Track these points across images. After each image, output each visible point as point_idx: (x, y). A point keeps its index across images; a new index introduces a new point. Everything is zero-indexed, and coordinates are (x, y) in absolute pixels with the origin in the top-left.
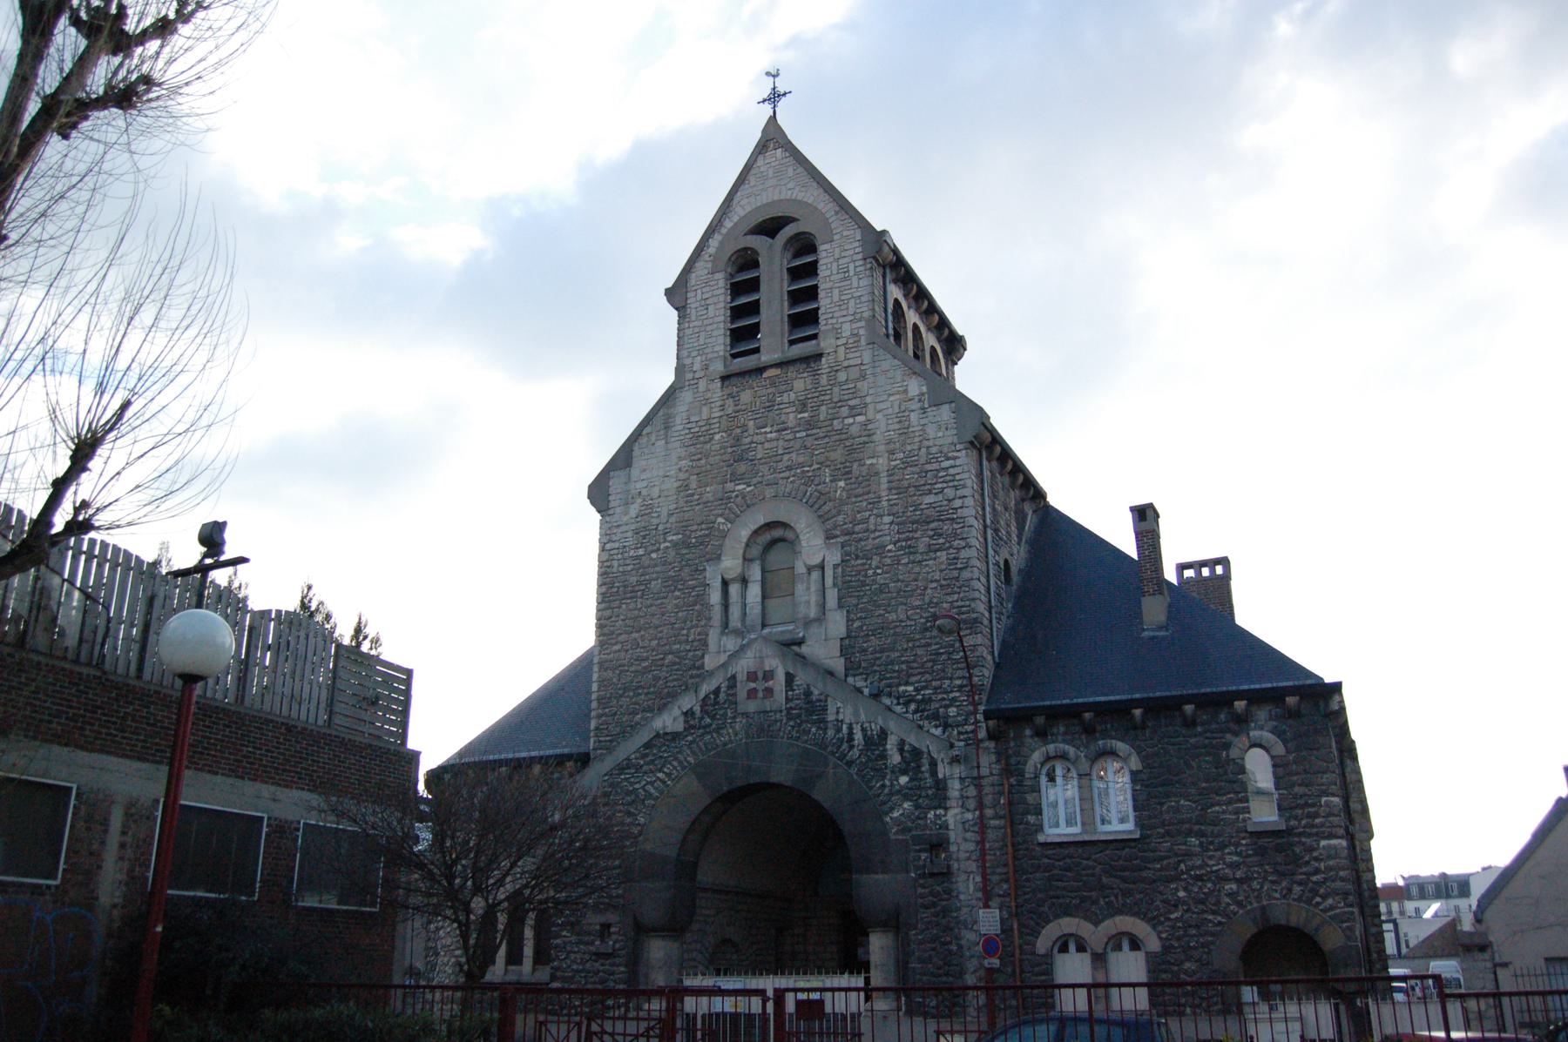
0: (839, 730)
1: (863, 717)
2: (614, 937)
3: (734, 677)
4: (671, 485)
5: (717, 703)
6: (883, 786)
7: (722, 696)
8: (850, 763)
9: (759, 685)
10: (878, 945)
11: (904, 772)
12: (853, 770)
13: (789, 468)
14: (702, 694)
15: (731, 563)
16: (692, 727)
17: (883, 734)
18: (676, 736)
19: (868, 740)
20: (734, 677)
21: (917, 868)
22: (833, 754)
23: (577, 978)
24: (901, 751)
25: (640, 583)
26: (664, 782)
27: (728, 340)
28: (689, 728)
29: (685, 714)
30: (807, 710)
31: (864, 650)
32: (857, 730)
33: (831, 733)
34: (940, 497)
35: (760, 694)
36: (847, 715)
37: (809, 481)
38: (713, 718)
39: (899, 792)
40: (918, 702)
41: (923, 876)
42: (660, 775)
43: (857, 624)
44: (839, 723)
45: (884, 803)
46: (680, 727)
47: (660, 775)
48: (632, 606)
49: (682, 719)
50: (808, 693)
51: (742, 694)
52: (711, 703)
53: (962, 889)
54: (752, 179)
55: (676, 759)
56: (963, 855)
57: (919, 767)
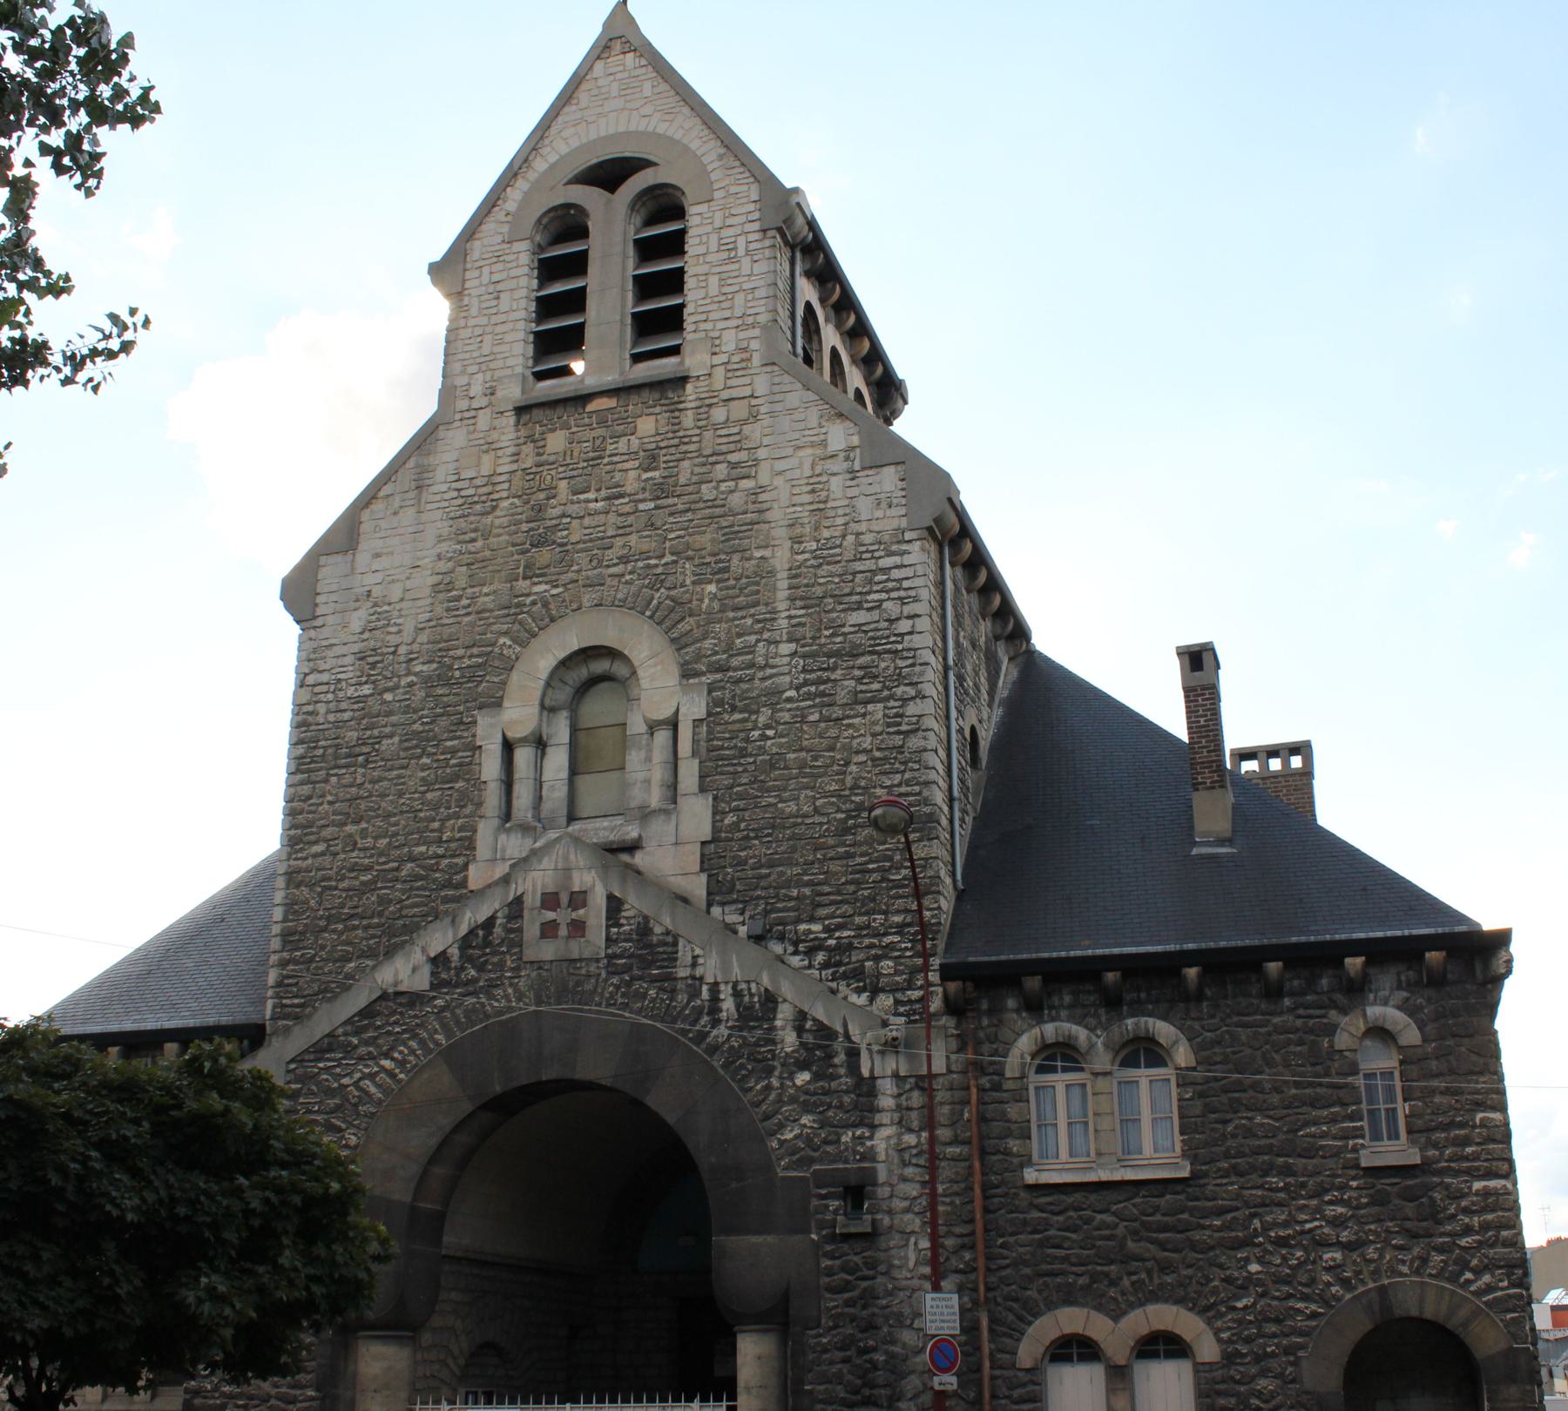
0: (695, 993)
1: (736, 972)
3: (519, 900)
5: (487, 943)
6: (768, 1088)
8: (714, 1049)
9: (562, 916)
11: (803, 1066)
15: (520, 712)
16: (447, 983)
17: (770, 1001)
18: (414, 999)
19: (746, 1015)
20: (519, 900)
21: (820, 1228)
27: (531, 348)
29: (434, 961)
32: (726, 992)
33: (682, 998)
36: (710, 969)
37: (658, 582)
38: (481, 968)
39: (793, 1100)
42: (387, 1063)
43: (730, 819)
45: (767, 1117)
46: (422, 982)
47: (387, 1063)
48: (347, 779)
49: (426, 970)
50: (644, 930)
51: (531, 930)
54: (583, 96)
55: (415, 1036)
57: (830, 1056)
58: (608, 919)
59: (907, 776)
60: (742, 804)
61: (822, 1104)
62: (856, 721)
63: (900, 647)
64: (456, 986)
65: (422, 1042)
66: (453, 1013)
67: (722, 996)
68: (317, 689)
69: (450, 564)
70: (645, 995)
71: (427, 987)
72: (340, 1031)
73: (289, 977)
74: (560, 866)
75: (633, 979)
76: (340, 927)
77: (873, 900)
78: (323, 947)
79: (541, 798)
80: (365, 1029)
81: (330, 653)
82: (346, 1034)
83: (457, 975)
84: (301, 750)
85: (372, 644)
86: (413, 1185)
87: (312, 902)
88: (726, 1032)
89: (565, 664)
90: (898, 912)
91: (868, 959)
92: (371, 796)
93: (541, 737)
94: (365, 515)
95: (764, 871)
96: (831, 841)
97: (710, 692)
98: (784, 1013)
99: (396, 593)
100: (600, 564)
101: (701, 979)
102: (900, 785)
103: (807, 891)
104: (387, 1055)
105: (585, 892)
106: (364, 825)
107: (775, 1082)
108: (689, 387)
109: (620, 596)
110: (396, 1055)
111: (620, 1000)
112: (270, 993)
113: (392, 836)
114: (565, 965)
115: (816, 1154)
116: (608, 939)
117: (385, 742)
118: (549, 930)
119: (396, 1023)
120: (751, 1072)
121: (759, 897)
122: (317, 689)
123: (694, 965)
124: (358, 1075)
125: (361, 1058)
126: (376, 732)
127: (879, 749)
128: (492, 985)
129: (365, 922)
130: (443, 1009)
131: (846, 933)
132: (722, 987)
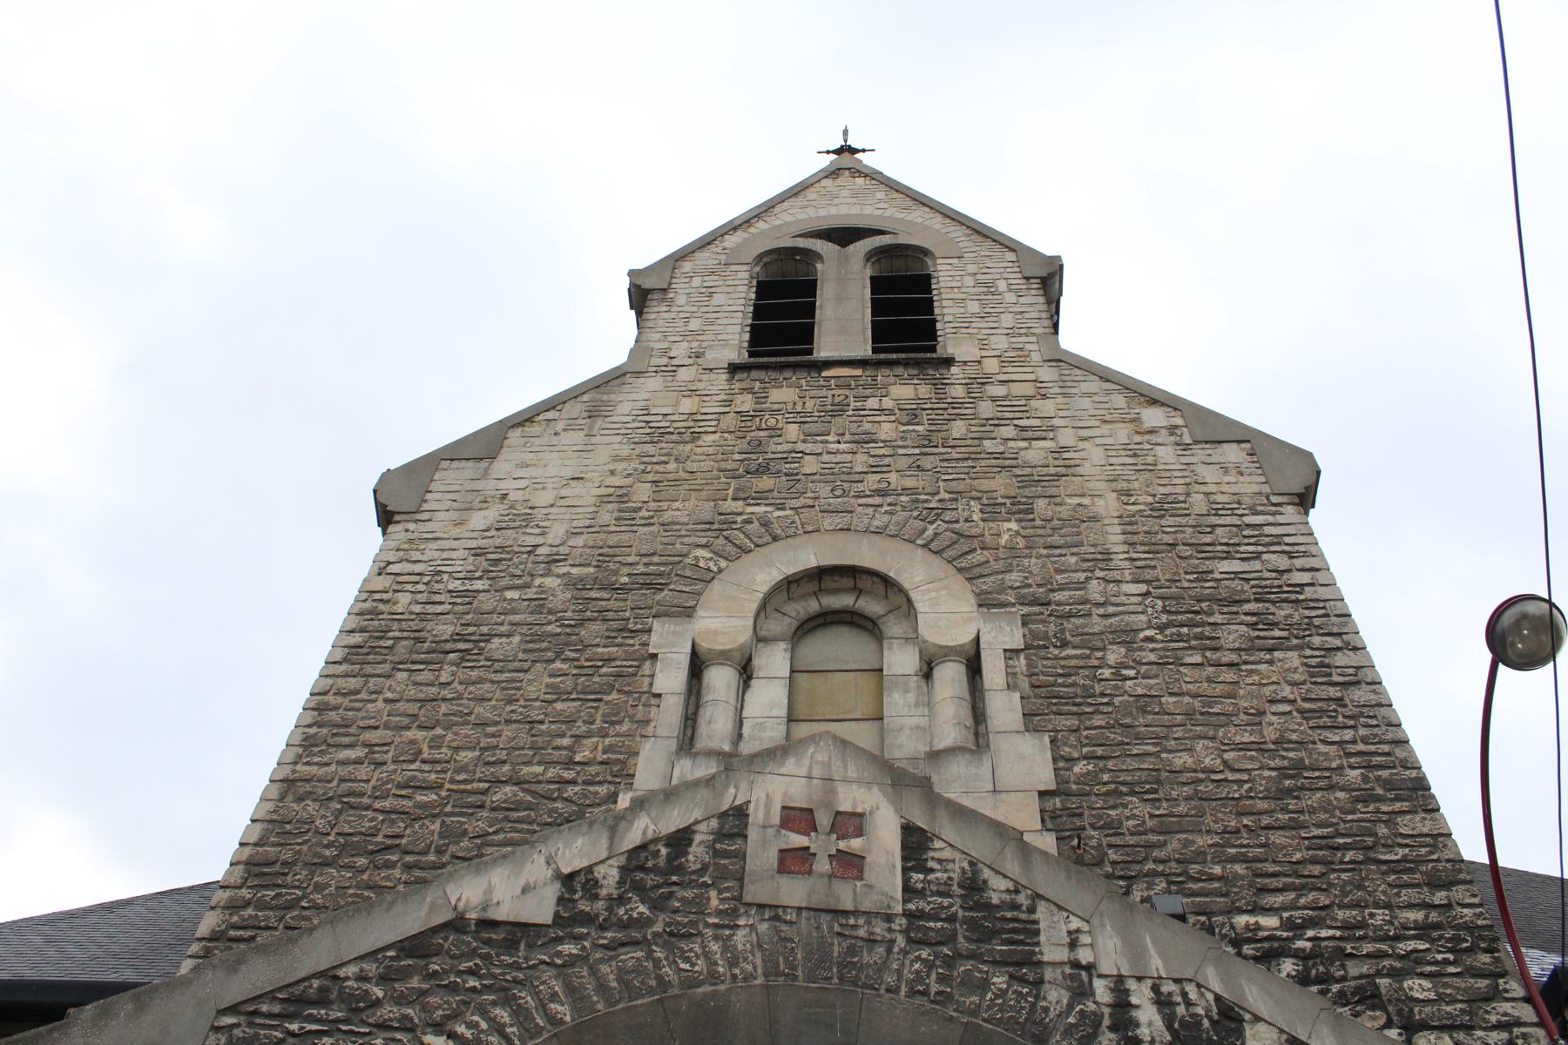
0: (1082, 992)
1: (1156, 965)
3: (740, 813)
4: (586, 494)
7: (697, 853)
9: (822, 844)
13: (882, 493)
14: (633, 836)
15: (723, 619)
16: (588, 919)
18: (519, 932)
20: (740, 813)
25: (458, 637)
27: (747, 337)
28: (568, 920)
29: (568, 880)
30: (972, 924)
31: (1113, 827)
32: (1141, 996)
33: (1056, 997)
34: (1256, 565)
35: (822, 865)
37: (936, 514)
38: (657, 906)
40: (1297, 955)
44: (1080, 975)
46: (541, 909)
48: (425, 676)
49: (552, 891)
50: (973, 885)
51: (761, 851)
52: (657, 868)
55: (507, 1000)
58: (904, 859)
59: (1362, 731)
60: (1099, 751)
62: (1262, 667)
63: (1301, 597)
65: (520, 1013)
66: (594, 972)
67: (1134, 1000)
68: (400, 579)
69: (628, 481)
70: (985, 985)
72: (352, 970)
73: (236, 927)
74: (816, 772)
75: (960, 955)
76: (362, 861)
77: (1360, 887)
78: (319, 888)
79: (740, 735)
80: (404, 974)
81: (435, 545)
82: (362, 978)
83: (609, 909)
84: (383, 582)
85: (498, 542)
87: (320, 823)
89: (790, 585)
90: (1410, 906)
91: (1379, 974)
92: (460, 698)
93: (750, 660)
94: (515, 436)
95: (1154, 838)
96: (1262, 805)
97: (1024, 624)
99: (543, 498)
100: (845, 494)
101: (1089, 968)
102: (1354, 742)
103: (1239, 869)
105: (861, 815)
106: (439, 731)
108: (954, 370)
109: (876, 523)
111: (934, 988)
112: (195, 948)
113: (483, 749)
114: (825, 919)
116: (908, 889)
117: (496, 641)
118: (794, 862)
119: (472, 972)
121: (1155, 874)
122: (400, 579)
123: (1073, 945)
125: (383, 1026)
126: (485, 629)
127: (1305, 700)
128: (675, 936)
129: (408, 858)
130: (572, 961)
131: (1324, 933)
132: (1131, 985)
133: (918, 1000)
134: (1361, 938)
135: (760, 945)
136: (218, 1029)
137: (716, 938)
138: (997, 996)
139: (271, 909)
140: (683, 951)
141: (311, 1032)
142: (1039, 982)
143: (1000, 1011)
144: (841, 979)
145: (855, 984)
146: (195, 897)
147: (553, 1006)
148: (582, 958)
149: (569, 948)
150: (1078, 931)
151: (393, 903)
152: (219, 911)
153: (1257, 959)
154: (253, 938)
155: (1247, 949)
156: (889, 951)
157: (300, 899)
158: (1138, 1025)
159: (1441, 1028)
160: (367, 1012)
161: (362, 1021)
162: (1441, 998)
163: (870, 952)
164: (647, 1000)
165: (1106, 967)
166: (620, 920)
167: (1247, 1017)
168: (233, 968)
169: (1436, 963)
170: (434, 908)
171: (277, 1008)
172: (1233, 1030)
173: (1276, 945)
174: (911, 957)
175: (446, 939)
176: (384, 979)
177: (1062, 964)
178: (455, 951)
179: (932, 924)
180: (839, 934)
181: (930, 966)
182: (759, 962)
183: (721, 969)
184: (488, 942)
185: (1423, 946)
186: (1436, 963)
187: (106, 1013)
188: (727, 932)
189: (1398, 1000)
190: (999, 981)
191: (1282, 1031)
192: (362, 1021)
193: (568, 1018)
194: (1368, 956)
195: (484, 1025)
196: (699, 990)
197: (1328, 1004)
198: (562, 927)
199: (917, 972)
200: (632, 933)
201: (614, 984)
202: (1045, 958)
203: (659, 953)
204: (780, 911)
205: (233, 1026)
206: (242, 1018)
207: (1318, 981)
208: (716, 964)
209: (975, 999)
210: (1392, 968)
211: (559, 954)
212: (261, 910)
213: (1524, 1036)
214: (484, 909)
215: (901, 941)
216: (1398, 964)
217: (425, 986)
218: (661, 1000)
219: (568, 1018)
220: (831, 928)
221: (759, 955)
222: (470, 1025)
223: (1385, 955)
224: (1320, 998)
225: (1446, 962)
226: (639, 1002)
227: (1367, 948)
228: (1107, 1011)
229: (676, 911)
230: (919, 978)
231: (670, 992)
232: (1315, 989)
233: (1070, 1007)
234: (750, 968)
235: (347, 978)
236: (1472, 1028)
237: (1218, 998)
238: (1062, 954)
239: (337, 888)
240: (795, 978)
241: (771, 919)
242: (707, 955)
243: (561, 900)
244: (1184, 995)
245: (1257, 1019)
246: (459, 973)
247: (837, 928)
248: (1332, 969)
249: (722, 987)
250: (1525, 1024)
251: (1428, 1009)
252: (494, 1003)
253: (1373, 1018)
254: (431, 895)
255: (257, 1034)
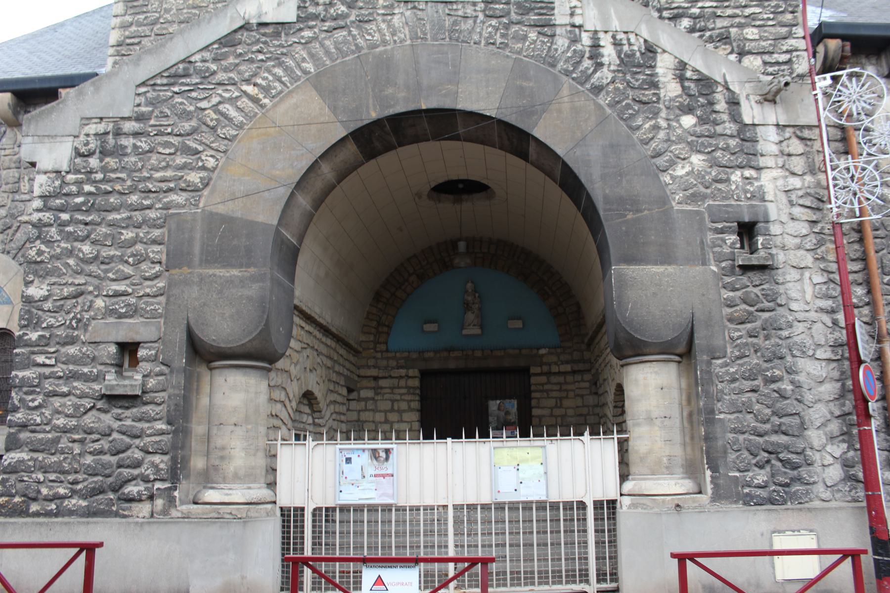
0: (575, 40)
1: (615, 25)
2: (145, 367)
6: (656, 128)
8: (598, 89)
10: (651, 387)
12: (604, 100)
16: (315, 17)
17: (650, 50)
19: (626, 62)
22: (567, 73)
23: (64, 444)
24: (681, 79)
26: (255, 100)
32: (605, 40)
33: (561, 42)
39: (680, 140)
41: (731, 271)
42: (250, 89)
45: (658, 155)
47: (250, 89)
53: (793, 294)
55: (280, 64)
56: (791, 242)
57: (711, 103)
61: (710, 145)
64: (323, 21)
65: (287, 69)
66: (322, 45)
67: (602, 43)
70: (525, 38)
71: (295, 20)
72: (197, 57)
80: (225, 56)
83: (326, 10)
86: (279, 208)
88: (610, 76)
91: (732, 26)
98: (664, 66)
101: (580, 27)
104: (247, 81)
107: (663, 124)
110: (259, 81)
115: (709, 191)
119: (260, 52)
120: (638, 112)
124: (215, 100)
128: (362, 22)
132: (601, 35)
133: (491, 47)
134: (726, 7)
135: (407, 23)
136: (139, 95)
137: (384, 21)
138: (531, 44)
139: (145, 25)
140: (367, 30)
141: (185, 91)
142: (553, 36)
143: (533, 51)
144: (450, 39)
145: (457, 40)
146: (97, 16)
147: (304, 65)
148: (315, 38)
149: (307, 34)
150: (575, 7)
151: (210, 19)
152: (117, 30)
153: (669, 19)
154: (140, 42)
155: (666, 14)
156: (475, 22)
157: (158, 18)
158: (603, 56)
159: (757, 54)
160: (212, 77)
161: (209, 83)
162: (761, 38)
163: (465, 23)
164: (351, 57)
165: (589, 26)
166: (332, 15)
167: (659, 50)
168: (137, 62)
169: (763, 20)
170: (232, 20)
171: (165, 81)
172: (652, 58)
173: (681, 11)
174: (487, 24)
175: (242, 35)
176: (215, 60)
177: (566, 25)
178: (249, 41)
179: (497, 6)
180: (449, 15)
181: (497, 29)
182: (407, 32)
183: (388, 38)
184: (264, 35)
185: (758, 10)
186: (763, 20)
187: (81, 93)
188: (389, 17)
189: (739, 40)
190: (533, 35)
191: (676, 58)
192: (209, 83)
193: (312, 70)
194: (729, 16)
195: (271, 78)
196: (377, 50)
197: (702, 43)
198: (302, 22)
199: (490, 33)
200: (339, 23)
201: (333, 50)
202: (557, 23)
203: (355, 32)
204: (416, 4)
205: (145, 93)
206: (149, 88)
207: (700, 30)
208: (385, 35)
209: (520, 45)
210: (740, 23)
211: (303, 37)
212: (140, 26)
213: (798, 56)
214: (259, 17)
215: (481, 16)
216: (743, 21)
217: (237, 61)
218: (358, 57)
219: (312, 70)
220: (444, 11)
221: (407, 29)
222: (264, 79)
223: (737, 16)
224: (699, 40)
225: (769, 19)
226: (347, 58)
227: (729, 12)
228: (588, 49)
229: (361, 8)
230: (491, 36)
231: (363, 52)
232: (697, 34)
233: (569, 47)
234: (402, 36)
235: (196, 62)
236: (773, 53)
237: (645, 41)
238: (566, 20)
239: (177, 10)
240: (426, 39)
241: (412, 8)
242: (379, 30)
243: (299, 7)
244: (629, 40)
245: (664, 51)
246: (253, 52)
247: (447, 11)
248: (708, 24)
249: (389, 47)
250: (800, 50)
251: (753, 44)
252: (274, 66)
253: (725, 49)
254: (230, 12)
255: (159, 95)
